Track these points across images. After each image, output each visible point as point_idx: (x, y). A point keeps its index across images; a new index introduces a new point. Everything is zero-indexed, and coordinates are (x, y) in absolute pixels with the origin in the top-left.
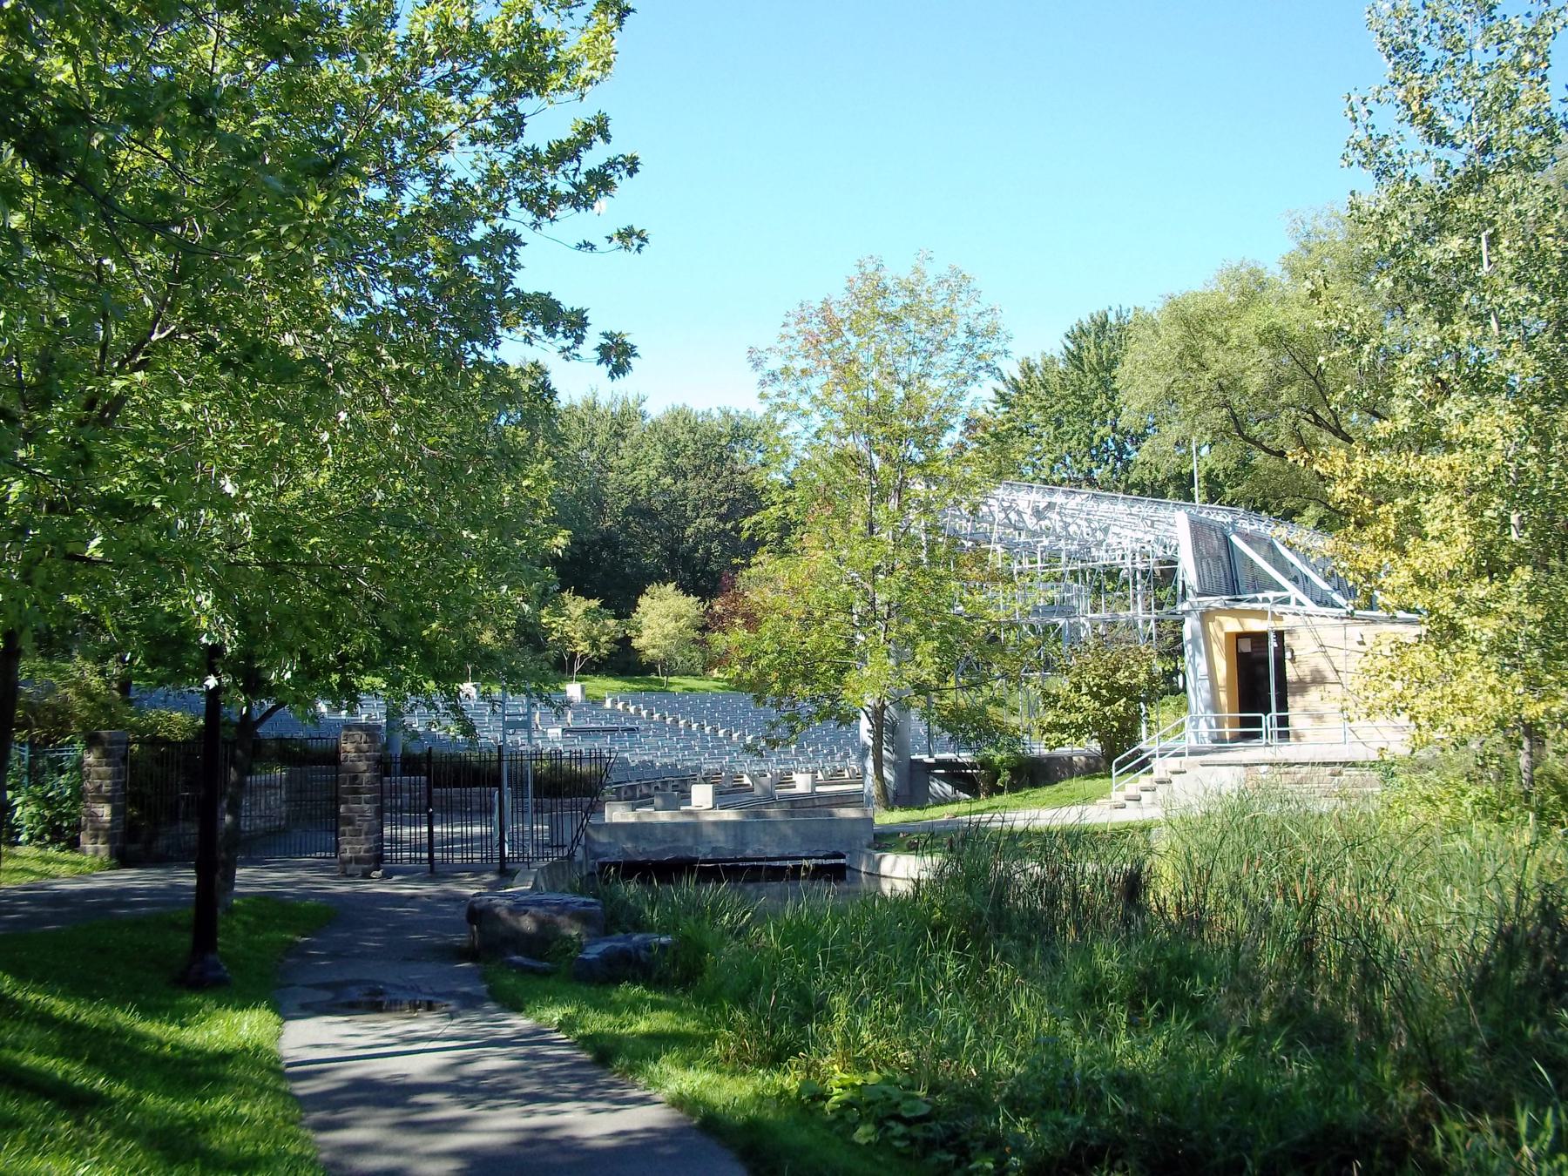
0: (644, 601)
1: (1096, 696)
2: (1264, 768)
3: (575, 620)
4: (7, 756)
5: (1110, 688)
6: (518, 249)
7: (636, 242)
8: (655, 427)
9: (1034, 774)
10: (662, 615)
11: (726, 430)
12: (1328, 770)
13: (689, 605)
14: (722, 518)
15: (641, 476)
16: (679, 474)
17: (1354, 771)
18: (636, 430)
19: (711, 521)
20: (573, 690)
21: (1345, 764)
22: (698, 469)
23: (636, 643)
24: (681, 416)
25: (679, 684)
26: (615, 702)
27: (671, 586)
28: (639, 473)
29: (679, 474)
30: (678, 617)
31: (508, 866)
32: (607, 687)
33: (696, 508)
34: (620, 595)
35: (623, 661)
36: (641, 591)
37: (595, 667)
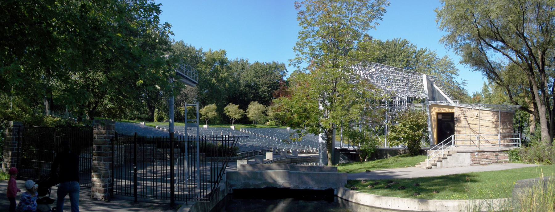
0: (250, 106)
1: (410, 128)
2: (476, 153)
3: (232, 110)
4: (554, 107)
5: (417, 125)
6: (203, 52)
7: (259, 74)
8: (252, 66)
9: (378, 154)
10: (254, 109)
11: (268, 68)
12: (495, 154)
13: (261, 106)
14: (268, 87)
15: (248, 79)
16: (258, 77)
17: (502, 154)
18: (247, 67)
19: (266, 88)
20: (232, 127)
21: (499, 151)
22: (262, 76)
23: (248, 116)
24: (257, 63)
25: (258, 126)
26: (242, 130)
27: (256, 102)
28: (248, 77)
29: (258, 77)
30: (258, 109)
31: (176, 202)
32: (242, 128)
33: (262, 85)
34: (244, 106)
35: (244, 120)
36: (249, 104)
37: (237, 122)
